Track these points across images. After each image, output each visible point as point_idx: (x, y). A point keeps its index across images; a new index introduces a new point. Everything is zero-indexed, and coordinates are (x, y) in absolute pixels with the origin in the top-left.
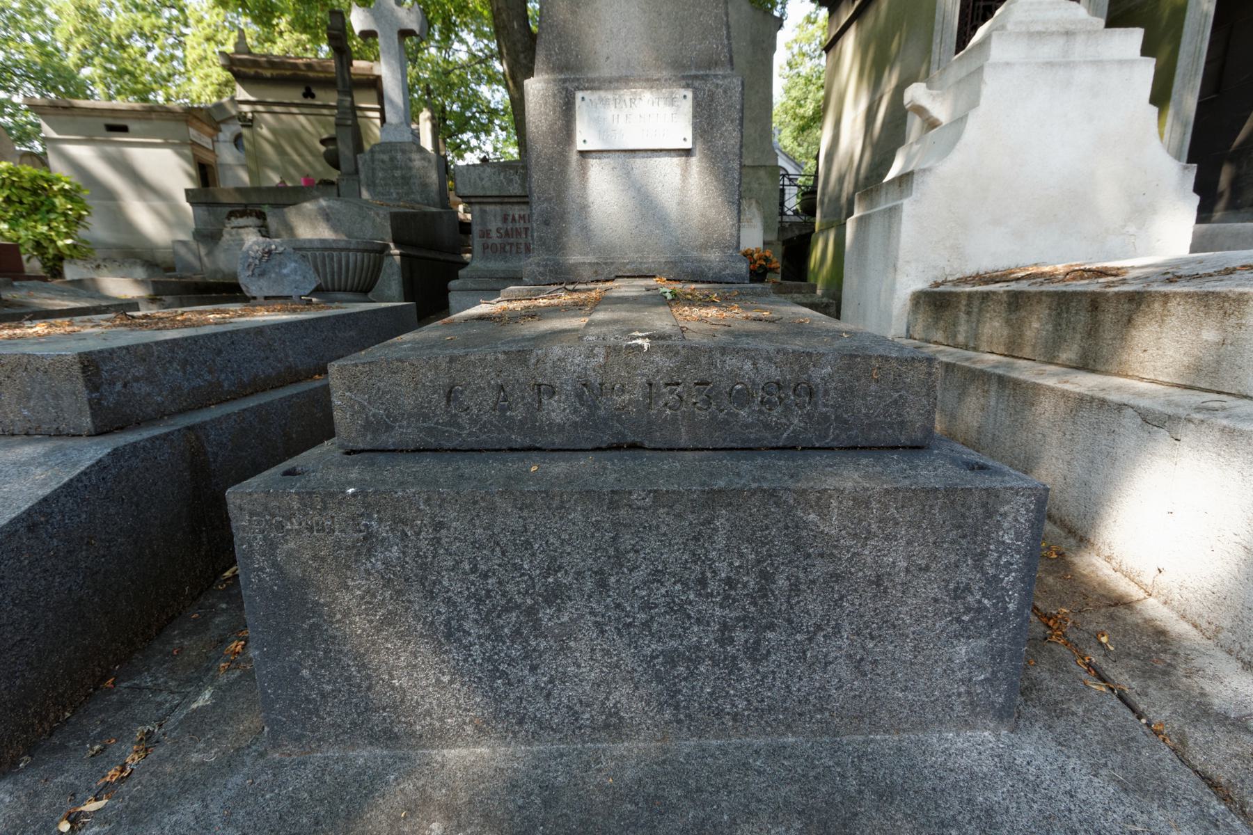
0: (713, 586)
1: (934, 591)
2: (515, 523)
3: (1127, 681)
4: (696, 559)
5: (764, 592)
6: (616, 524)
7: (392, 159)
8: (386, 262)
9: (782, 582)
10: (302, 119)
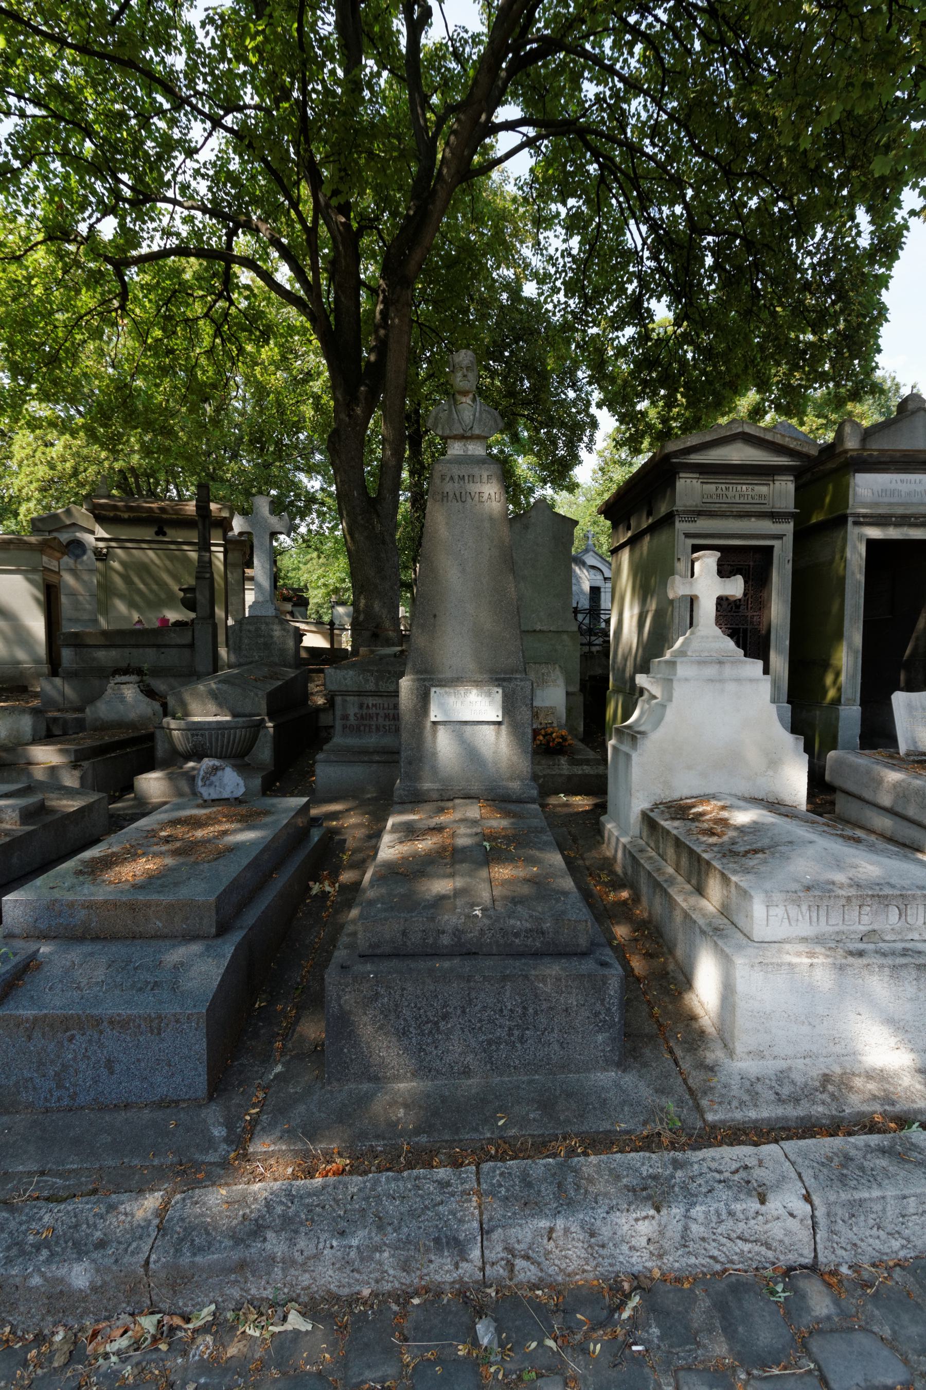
0: (505, 1012)
1: (587, 1014)
2: (432, 988)
3: (679, 1053)
4: (499, 1002)
5: (524, 1014)
6: (469, 988)
7: (257, 629)
8: (262, 733)
9: (531, 1011)
10: (151, 553)
